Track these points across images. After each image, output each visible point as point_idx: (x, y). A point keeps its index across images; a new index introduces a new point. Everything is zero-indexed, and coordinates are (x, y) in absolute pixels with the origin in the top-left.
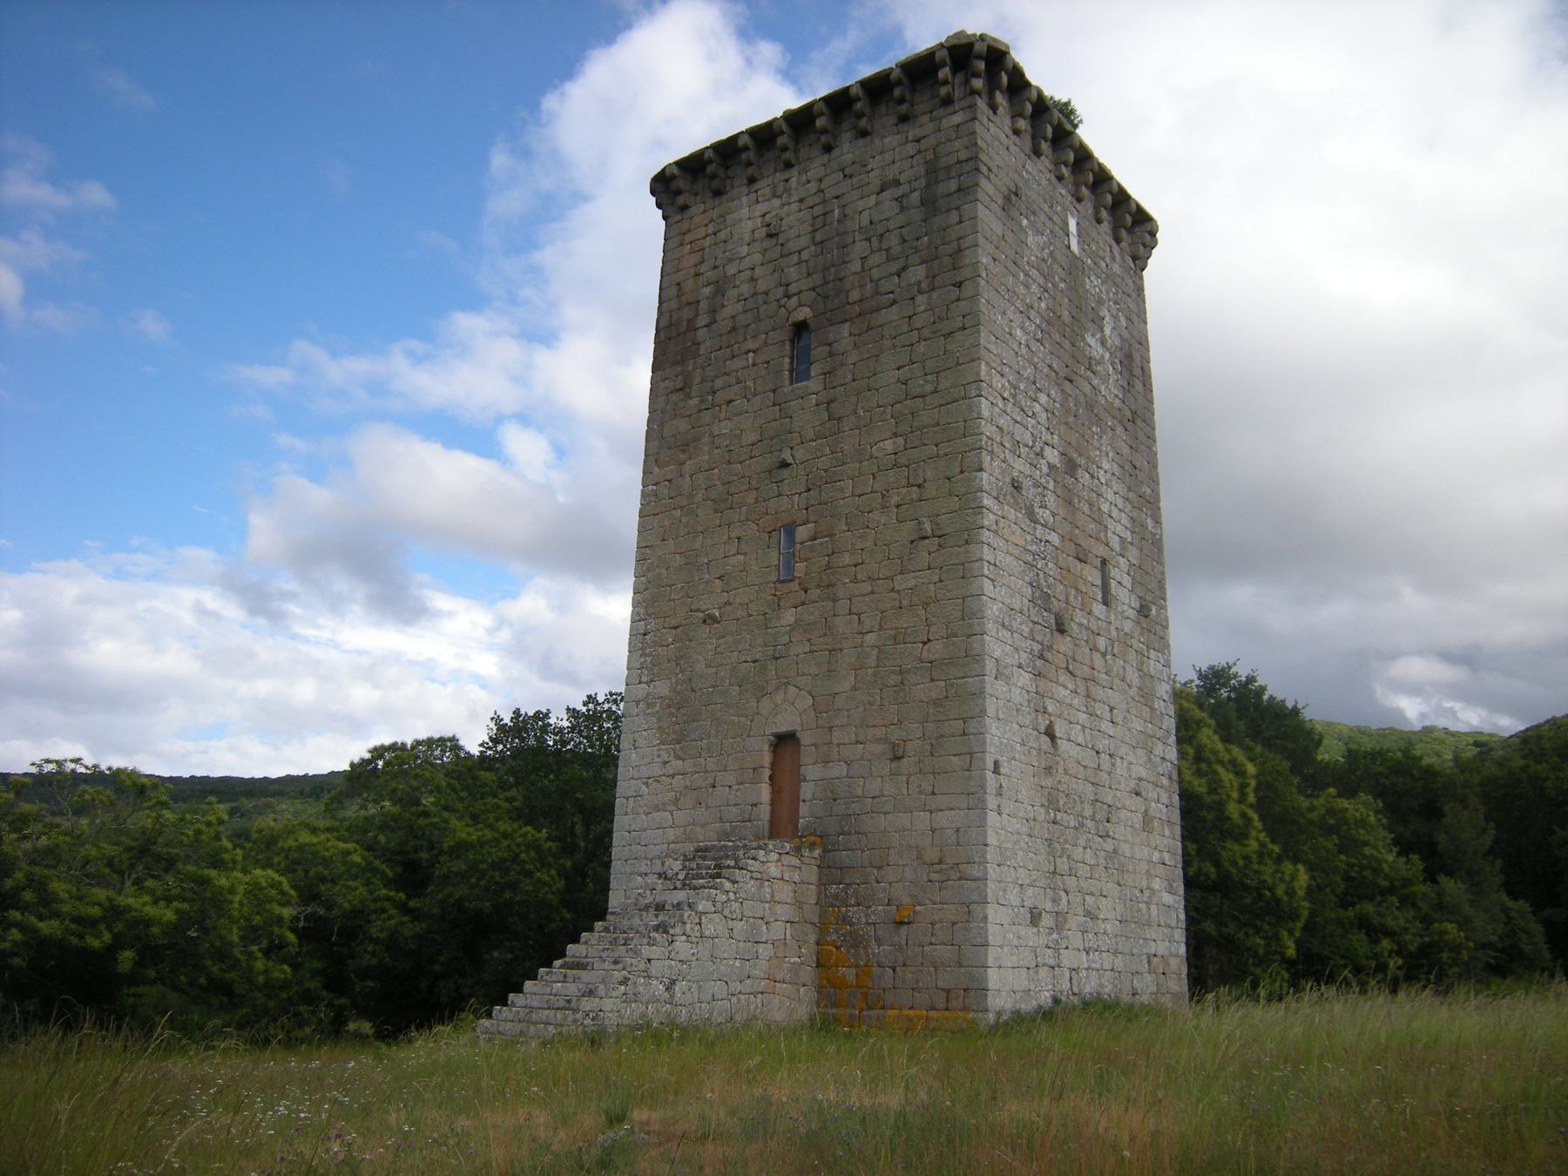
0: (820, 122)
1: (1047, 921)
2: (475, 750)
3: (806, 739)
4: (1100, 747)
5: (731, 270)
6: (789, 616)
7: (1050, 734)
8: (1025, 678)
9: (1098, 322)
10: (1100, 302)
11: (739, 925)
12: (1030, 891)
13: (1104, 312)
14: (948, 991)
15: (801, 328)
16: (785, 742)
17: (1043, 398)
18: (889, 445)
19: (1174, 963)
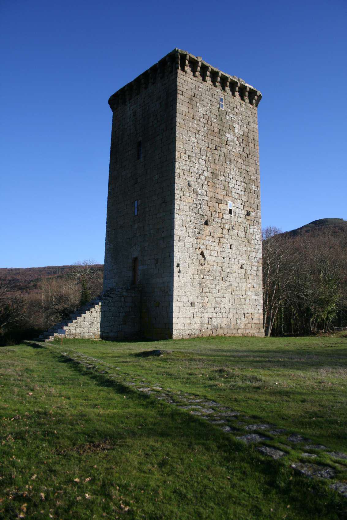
0: (143, 81)
1: (197, 305)
2: (100, 260)
3: (139, 259)
4: (225, 256)
5: (126, 127)
6: (136, 226)
7: (202, 254)
8: (191, 240)
9: (232, 129)
10: (233, 122)
11: (113, 308)
12: (191, 298)
13: (236, 125)
14: (165, 324)
15: (140, 144)
16: (135, 259)
17: (204, 157)
18: (157, 177)
19: (256, 316)
